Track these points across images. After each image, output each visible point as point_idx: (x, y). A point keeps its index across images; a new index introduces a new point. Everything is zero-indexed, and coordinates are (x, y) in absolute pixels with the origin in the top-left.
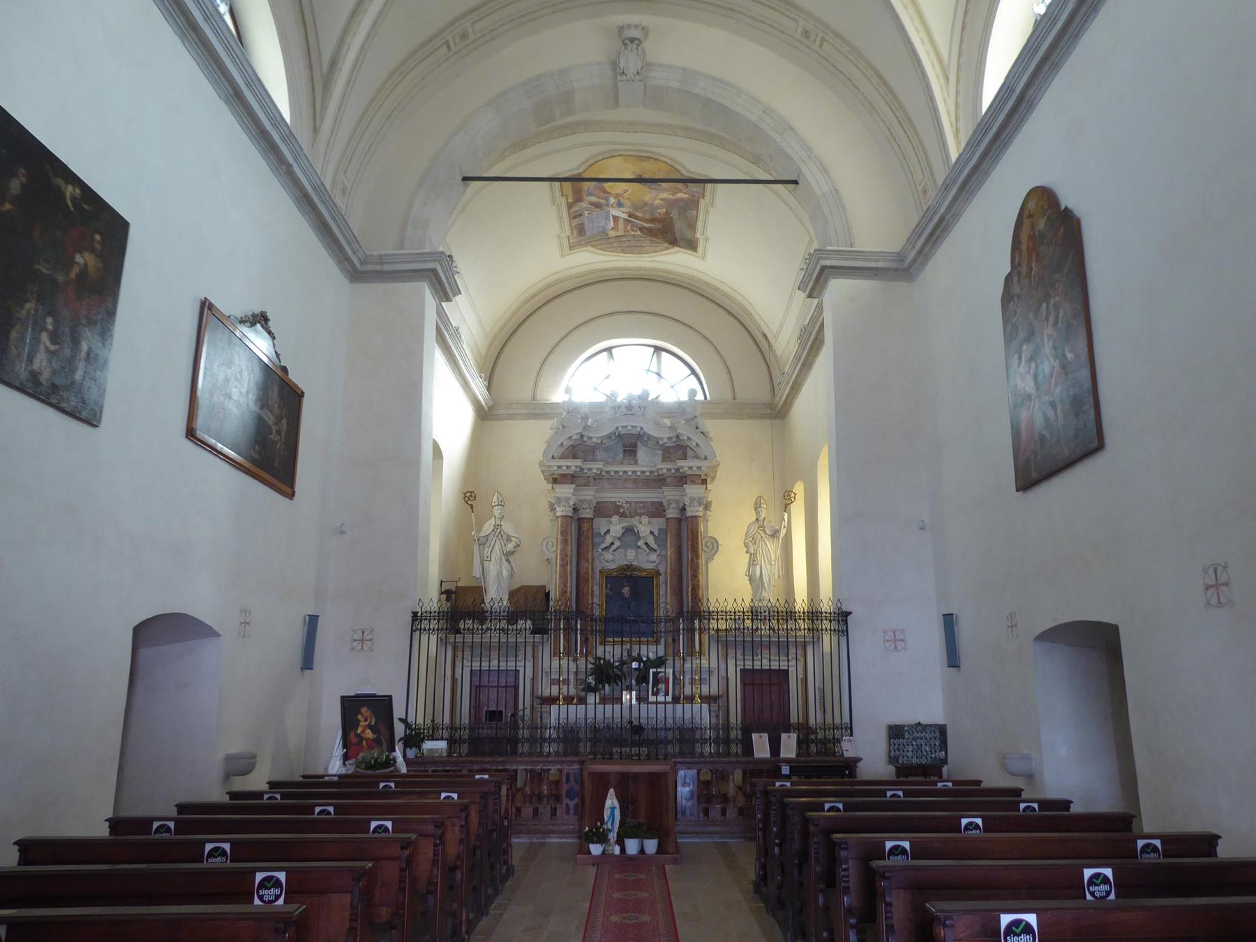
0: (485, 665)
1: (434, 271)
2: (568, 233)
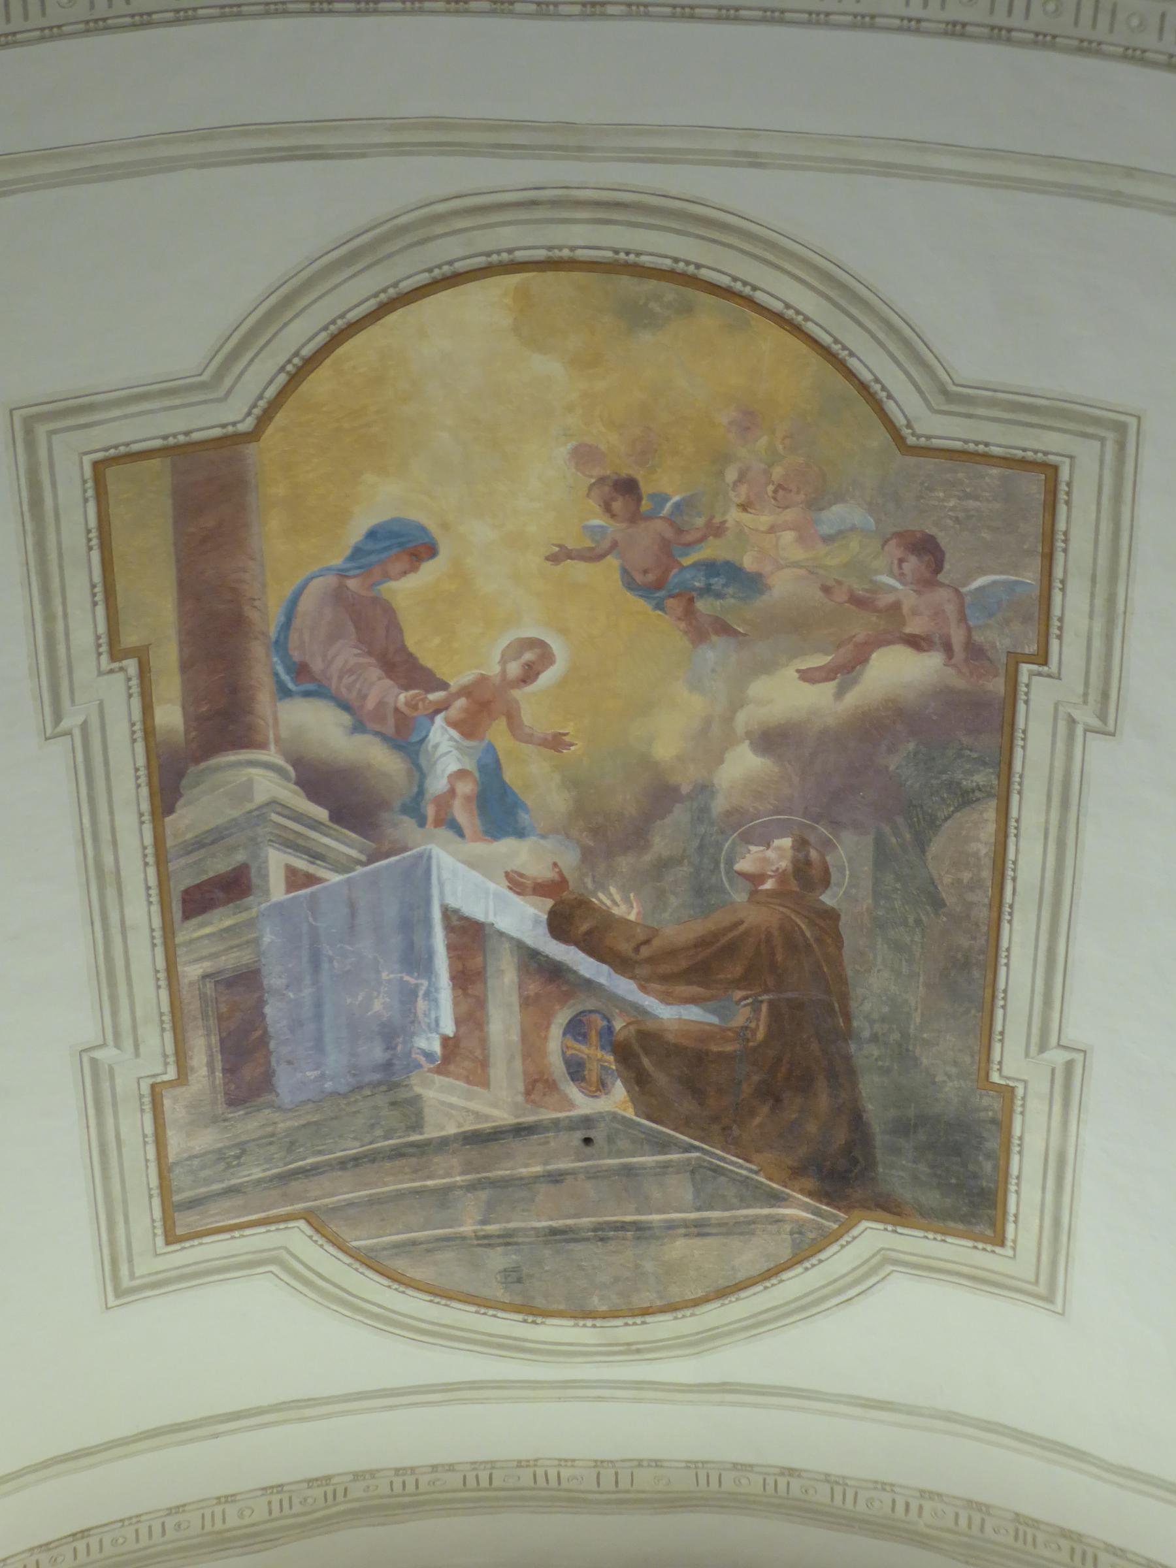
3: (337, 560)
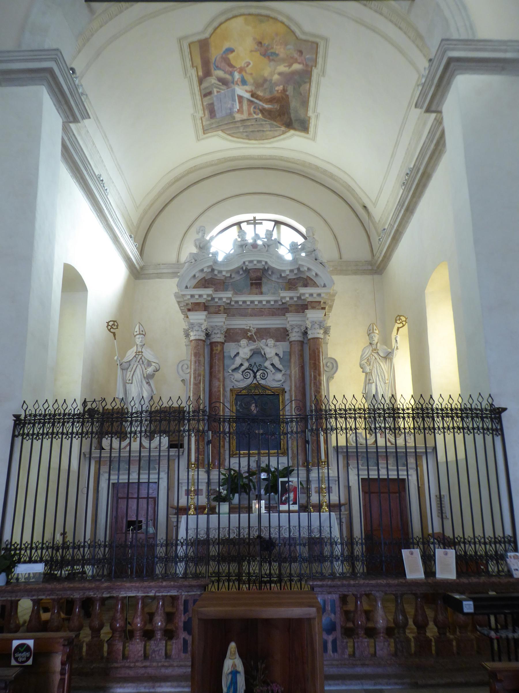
0: (123, 479)
1: (50, 71)
2: (201, 114)
3: (222, 52)
